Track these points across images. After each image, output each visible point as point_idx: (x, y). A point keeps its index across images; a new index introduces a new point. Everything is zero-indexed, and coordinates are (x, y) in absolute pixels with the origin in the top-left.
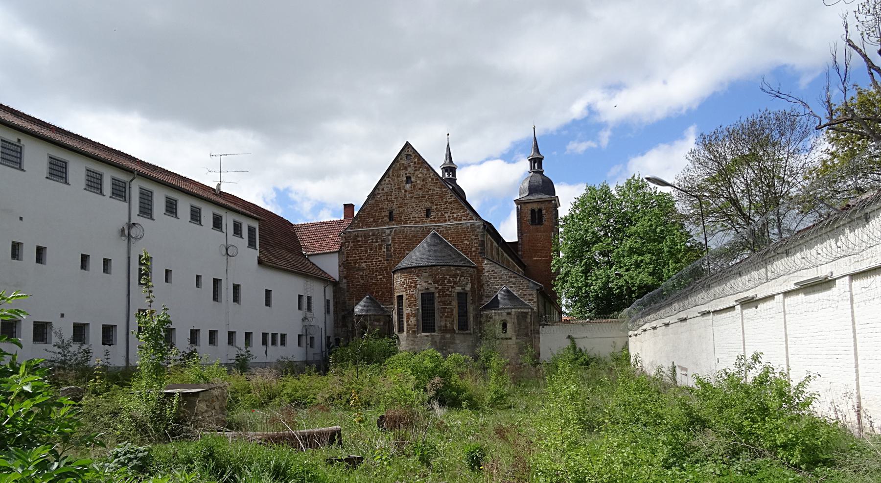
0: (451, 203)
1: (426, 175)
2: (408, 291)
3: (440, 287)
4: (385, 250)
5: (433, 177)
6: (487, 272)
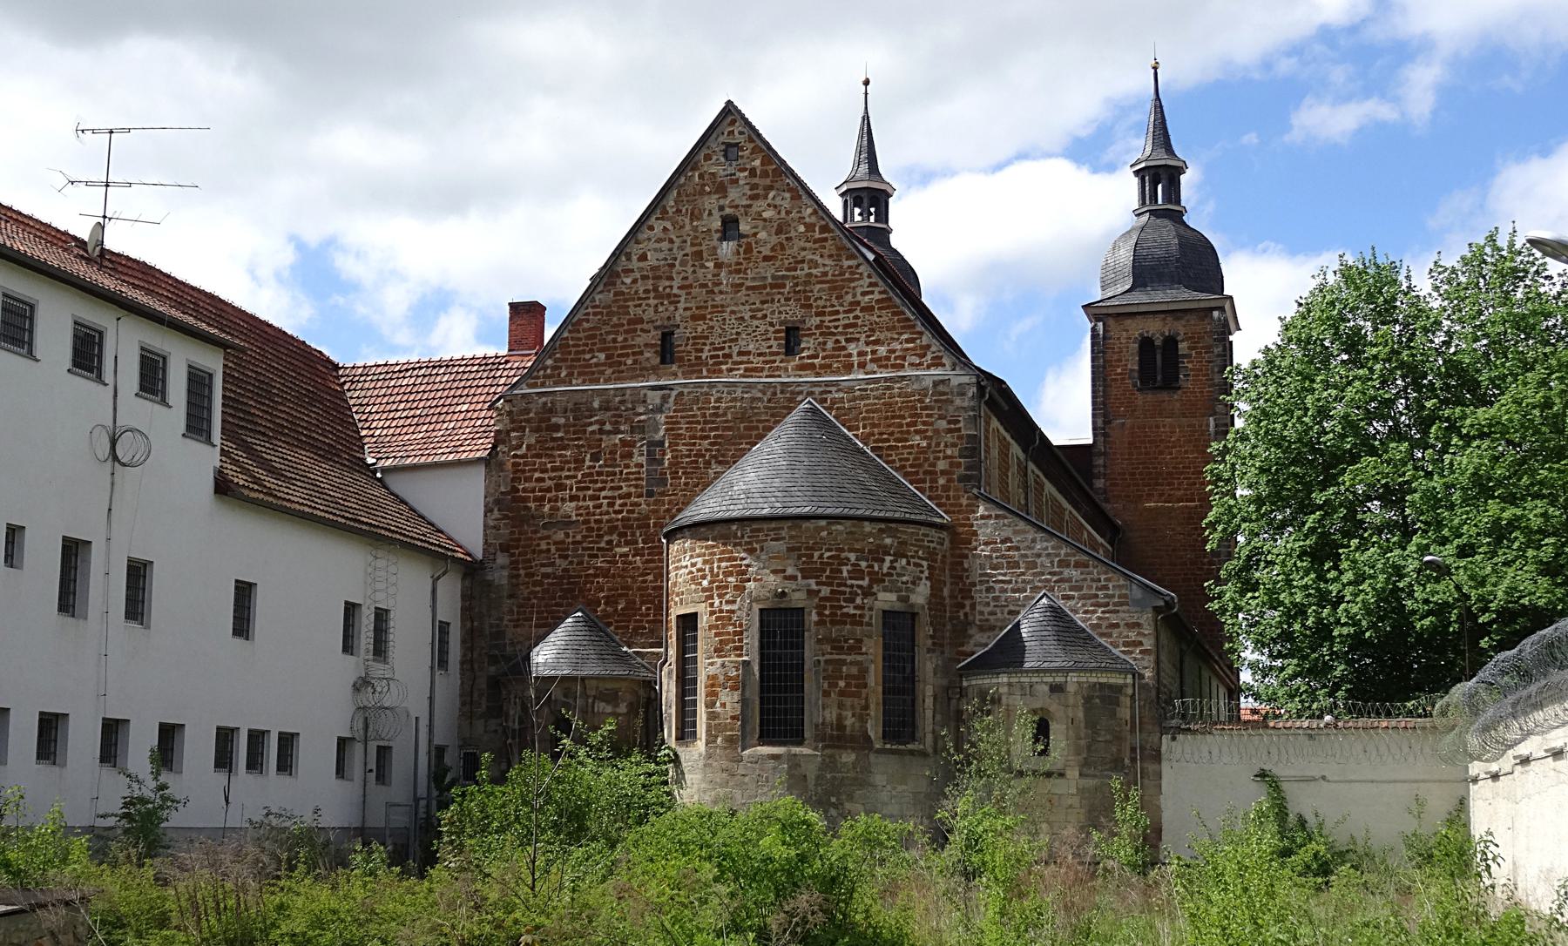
0: (868, 309)
1: (788, 213)
2: (717, 602)
3: (825, 591)
4: (643, 460)
5: (813, 219)
6: (986, 544)
